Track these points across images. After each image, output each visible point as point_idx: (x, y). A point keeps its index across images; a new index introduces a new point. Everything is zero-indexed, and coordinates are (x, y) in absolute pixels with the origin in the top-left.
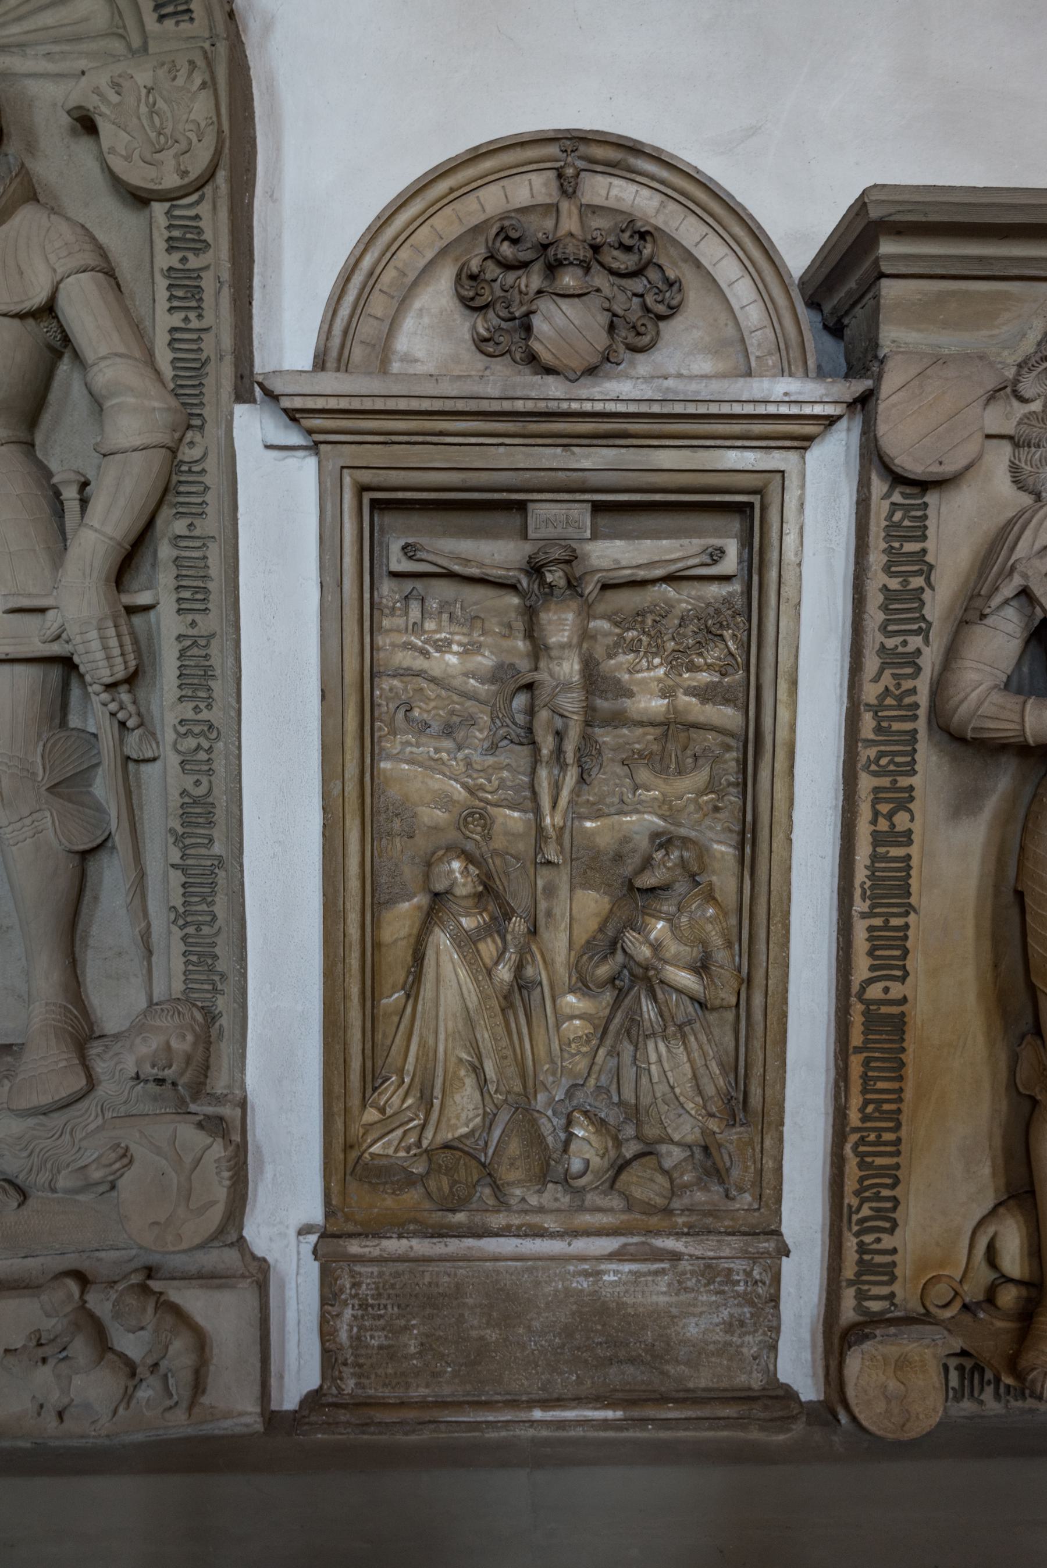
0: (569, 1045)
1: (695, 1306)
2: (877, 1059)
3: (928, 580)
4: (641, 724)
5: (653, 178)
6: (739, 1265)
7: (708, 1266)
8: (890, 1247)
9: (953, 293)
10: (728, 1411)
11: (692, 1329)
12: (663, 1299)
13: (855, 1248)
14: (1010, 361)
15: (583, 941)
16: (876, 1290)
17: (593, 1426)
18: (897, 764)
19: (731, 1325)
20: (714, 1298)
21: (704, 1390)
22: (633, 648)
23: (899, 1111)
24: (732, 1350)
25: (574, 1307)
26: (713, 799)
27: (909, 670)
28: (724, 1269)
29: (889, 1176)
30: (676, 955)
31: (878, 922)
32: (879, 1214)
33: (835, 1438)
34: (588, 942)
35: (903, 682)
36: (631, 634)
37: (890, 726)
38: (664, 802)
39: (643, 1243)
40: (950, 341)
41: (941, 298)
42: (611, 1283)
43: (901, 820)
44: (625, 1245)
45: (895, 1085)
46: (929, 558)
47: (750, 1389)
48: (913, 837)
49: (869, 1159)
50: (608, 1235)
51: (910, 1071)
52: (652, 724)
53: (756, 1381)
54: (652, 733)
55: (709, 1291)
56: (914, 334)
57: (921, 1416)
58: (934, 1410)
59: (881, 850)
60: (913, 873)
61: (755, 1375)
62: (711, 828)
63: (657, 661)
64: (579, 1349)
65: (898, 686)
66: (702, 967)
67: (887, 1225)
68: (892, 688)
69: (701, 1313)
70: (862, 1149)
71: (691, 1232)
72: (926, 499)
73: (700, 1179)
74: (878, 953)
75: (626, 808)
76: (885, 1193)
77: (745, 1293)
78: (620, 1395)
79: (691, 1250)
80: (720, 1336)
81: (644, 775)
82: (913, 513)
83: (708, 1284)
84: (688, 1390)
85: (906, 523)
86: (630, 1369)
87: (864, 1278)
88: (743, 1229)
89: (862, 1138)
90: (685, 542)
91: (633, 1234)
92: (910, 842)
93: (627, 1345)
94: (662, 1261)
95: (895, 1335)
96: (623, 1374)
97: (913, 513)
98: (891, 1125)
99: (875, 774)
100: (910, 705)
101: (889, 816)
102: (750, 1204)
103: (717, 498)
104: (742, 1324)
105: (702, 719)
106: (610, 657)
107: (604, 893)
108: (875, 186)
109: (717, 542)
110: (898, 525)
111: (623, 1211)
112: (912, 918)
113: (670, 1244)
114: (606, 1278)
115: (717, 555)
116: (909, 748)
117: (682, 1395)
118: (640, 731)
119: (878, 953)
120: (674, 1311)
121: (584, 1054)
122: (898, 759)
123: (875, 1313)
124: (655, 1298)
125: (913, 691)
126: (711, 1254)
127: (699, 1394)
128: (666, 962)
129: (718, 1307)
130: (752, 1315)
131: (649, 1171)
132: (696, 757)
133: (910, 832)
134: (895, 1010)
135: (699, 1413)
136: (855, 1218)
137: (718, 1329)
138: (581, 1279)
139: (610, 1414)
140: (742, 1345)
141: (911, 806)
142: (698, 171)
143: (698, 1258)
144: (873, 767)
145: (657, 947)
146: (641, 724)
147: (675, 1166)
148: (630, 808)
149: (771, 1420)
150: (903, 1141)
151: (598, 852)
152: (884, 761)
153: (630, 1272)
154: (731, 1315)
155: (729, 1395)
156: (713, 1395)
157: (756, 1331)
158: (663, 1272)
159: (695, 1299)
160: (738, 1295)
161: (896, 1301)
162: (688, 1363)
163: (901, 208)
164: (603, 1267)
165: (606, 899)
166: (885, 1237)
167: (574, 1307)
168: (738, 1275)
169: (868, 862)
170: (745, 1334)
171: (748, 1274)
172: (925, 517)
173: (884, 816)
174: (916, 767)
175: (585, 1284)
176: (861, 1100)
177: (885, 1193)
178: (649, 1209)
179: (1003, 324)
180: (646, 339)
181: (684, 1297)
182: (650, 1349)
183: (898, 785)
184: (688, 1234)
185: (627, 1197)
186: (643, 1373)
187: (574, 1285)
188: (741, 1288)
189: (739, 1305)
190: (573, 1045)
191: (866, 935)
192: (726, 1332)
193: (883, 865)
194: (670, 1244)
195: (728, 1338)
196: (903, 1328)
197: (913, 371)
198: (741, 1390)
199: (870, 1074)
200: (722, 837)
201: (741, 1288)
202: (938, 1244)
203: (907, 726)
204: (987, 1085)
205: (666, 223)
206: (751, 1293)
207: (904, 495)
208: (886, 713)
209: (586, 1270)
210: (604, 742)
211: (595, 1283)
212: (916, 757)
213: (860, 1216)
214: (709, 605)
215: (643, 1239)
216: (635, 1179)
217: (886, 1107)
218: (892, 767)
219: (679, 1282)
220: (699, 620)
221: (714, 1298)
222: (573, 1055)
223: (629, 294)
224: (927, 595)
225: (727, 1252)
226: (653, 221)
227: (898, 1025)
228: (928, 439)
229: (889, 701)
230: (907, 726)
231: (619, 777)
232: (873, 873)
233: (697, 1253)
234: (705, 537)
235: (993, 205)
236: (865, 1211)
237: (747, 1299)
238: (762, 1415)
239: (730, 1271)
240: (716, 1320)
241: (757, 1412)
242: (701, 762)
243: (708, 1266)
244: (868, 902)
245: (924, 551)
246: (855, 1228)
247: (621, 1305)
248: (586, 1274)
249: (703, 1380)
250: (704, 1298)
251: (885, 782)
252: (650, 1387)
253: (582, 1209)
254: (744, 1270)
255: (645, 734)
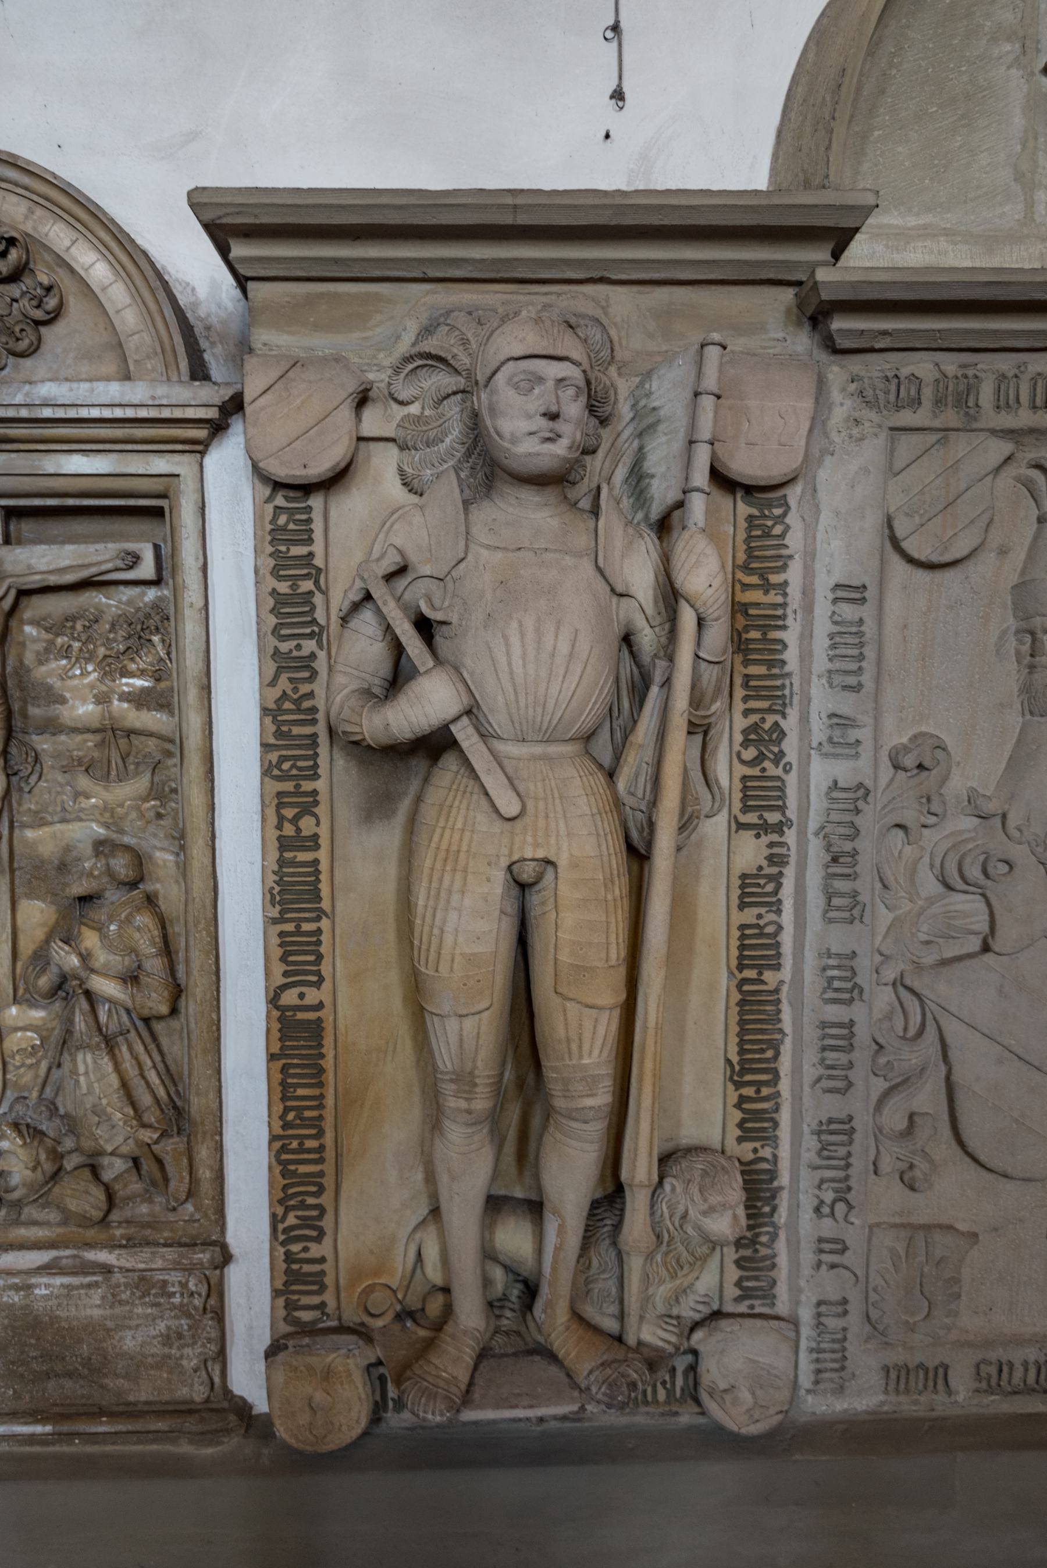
0: (13, 1058)
1: (130, 1318)
2: (297, 1066)
3: (317, 583)
4: (76, 730)
5: (16, 184)
6: (175, 1277)
7: (142, 1279)
8: (318, 1255)
9: (321, 296)
10: (161, 1425)
11: (130, 1342)
12: (97, 1313)
13: (283, 1257)
14: (386, 363)
15: (30, 952)
16: (305, 1300)
17: (18, 1441)
18: (300, 769)
19: (168, 1337)
20: (149, 1311)
21: (146, 1403)
22: (66, 652)
23: (321, 1117)
24: (171, 1363)
25: (6, 1321)
26: (154, 806)
27: (306, 674)
28: (158, 1281)
29: (314, 1184)
30: (106, 964)
31: (290, 927)
32: (305, 1222)
33: (265, 1451)
34: (35, 953)
35: (300, 686)
36: (59, 640)
37: (290, 730)
38: (105, 809)
39: (75, 1256)
40: (322, 343)
41: (310, 301)
42: (43, 1296)
43: (307, 824)
44: (57, 1259)
45: (316, 1092)
46: (319, 562)
47: (192, 1402)
48: (320, 841)
49: (292, 1167)
50: (40, 1249)
51: (330, 1077)
52: (95, 731)
53: (198, 1393)
54: (91, 741)
55: (145, 1303)
56: (286, 337)
57: (344, 1428)
58: (357, 1422)
59: (288, 855)
60: (322, 877)
61: (196, 1387)
62: (155, 835)
63: (90, 668)
64: (13, 1363)
65: (295, 690)
66: (132, 978)
67: (314, 1233)
68: (289, 692)
69: (138, 1326)
70: (284, 1157)
71: (130, 1244)
72: (310, 503)
73: (147, 1191)
74: (291, 958)
75: (68, 816)
76: (310, 1201)
77: (182, 1305)
78: (57, 1410)
79: (123, 1263)
80: (157, 1349)
81: (84, 782)
82: (298, 517)
83: (143, 1296)
84: (129, 1404)
85: (291, 526)
86: (68, 1384)
87: (294, 1288)
88: (184, 1240)
89: (283, 1147)
90: (100, 546)
91: (67, 1247)
92: (317, 847)
93: (63, 1359)
94: (94, 1274)
95: (308, 1346)
96: (63, 1387)
97: (298, 517)
98: (313, 1132)
99: (278, 779)
100: (308, 709)
101: (295, 820)
102: (192, 1215)
103: (132, 502)
104: (180, 1336)
105: (138, 725)
106: (41, 663)
107: (52, 903)
108: (197, 188)
109: (131, 546)
110: (284, 529)
111: (59, 1225)
112: (325, 924)
113: (102, 1256)
114: (37, 1291)
115: (135, 560)
116: (311, 752)
117: (121, 1408)
118: (79, 738)
119: (291, 958)
120: (110, 1324)
121: (31, 1066)
122: (300, 764)
123: (306, 1324)
124: (89, 1312)
125: (311, 695)
126: (142, 1266)
127: (140, 1407)
128: (93, 971)
129: (154, 1319)
130: (190, 1327)
131: (83, 1184)
132: (137, 764)
133: (315, 837)
134: (311, 1016)
135: (130, 1428)
136: (281, 1227)
137: (155, 1342)
138: (12, 1293)
139: (39, 1429)
140: (182, 1357)
141: (316, 810)
142: (55, 176)
143: (128, 1270)
144: (276, 772)
145: (85, 958)
146: (76, 730)
147: (116, 1179)
148: (73, 816)
149: (202, 1433)
150: (328, 1149)
151: (42, 862)
152: (286, 766)
153: (62, 1285)
154: (168, 1328)
155: (171, 1408)
156: (154, 1408)
157: (195, 1343)
158: (96, 1285)
159: (131, 1311)
160: (174, 1307)
161: (328, 1310)
162: (127, 1376)
163: (228, 211)
164: (33, 1281)
165: (53, 909)
166: (312, 1245)
167: (6, 1321)
168: (173, 1286)
169: (276, 868)
170: (183, 1346)
171: (184, 1285)
172: (309, 521)
173: (290, 821)
174: (319, 771)
175: (16, 1298)
176: (281, 1107)
177: (310, 1201)
178: (84, 1221)
179: (377, 326)
180: (23, 345)
181: (118, 1310)
182: (87, 1362)
183: (302, 789)
184: (121, 1246)
185: (63, 1210)
186: (82, 1387)
187: (5, 1299)
188: (177, 1300)
189: (176, 1317)
190: (17, 1057)
191: (279, 941)
192: (164, 1345)
193: (291, 870)
194: (102, 1256)
195: (166, 1350)
196: (317, 1339)
197: (274, 375)
198: (179, 1403)
199: (289, 1081)
200: (166, 844)
201: (177, 1300)
202: (371, 1252)
203: (307, 730)
204: (417, 1090)
205: (35, 229)
206: (187, 1305)
207: (287, 498)
208: (285, 718)
209: (16, 1285)
210: (43, 750)
211: (26, 1297)
212: (319, 761)
213: (286, 1224)
214: (138, 609)
215: (75, 1252)
216: (69, 1192)
217: (308, 1114)
218: (294, 772)
219: (113, 1295)
220: (130, 625)
221: (149, 1311)
222: (18, 1068)
223: (8, 300)
224: (318, 599)
225: (159, 1264)
226: (22, 227)
227: (316, 1030)
228: (298, 442)
229: (288, 705)
230: (307, 730)
231: (61, 786)
232: (281, 879)
233: (128, 1265)
234: (119, 541)
235: (319, 206)
236: (291, 1220)
237: (184, 1311)
238: (193, 1428)
239: (165, 1283)
240: (153, 1333)
241: (190, 1424)
242: (141, 768)
243: (142, 1279)
244: (278, 908)
245: (311, 555)
246: (282, 1237)
247: (54, 1319)
248: (17, 1288)
249: (143, 1393)
250: (139, 1310)
251: (289, 786)
252: (90, 1401)
253: (17, 1222)
254: (180, 1282)
255: (86, 741)
